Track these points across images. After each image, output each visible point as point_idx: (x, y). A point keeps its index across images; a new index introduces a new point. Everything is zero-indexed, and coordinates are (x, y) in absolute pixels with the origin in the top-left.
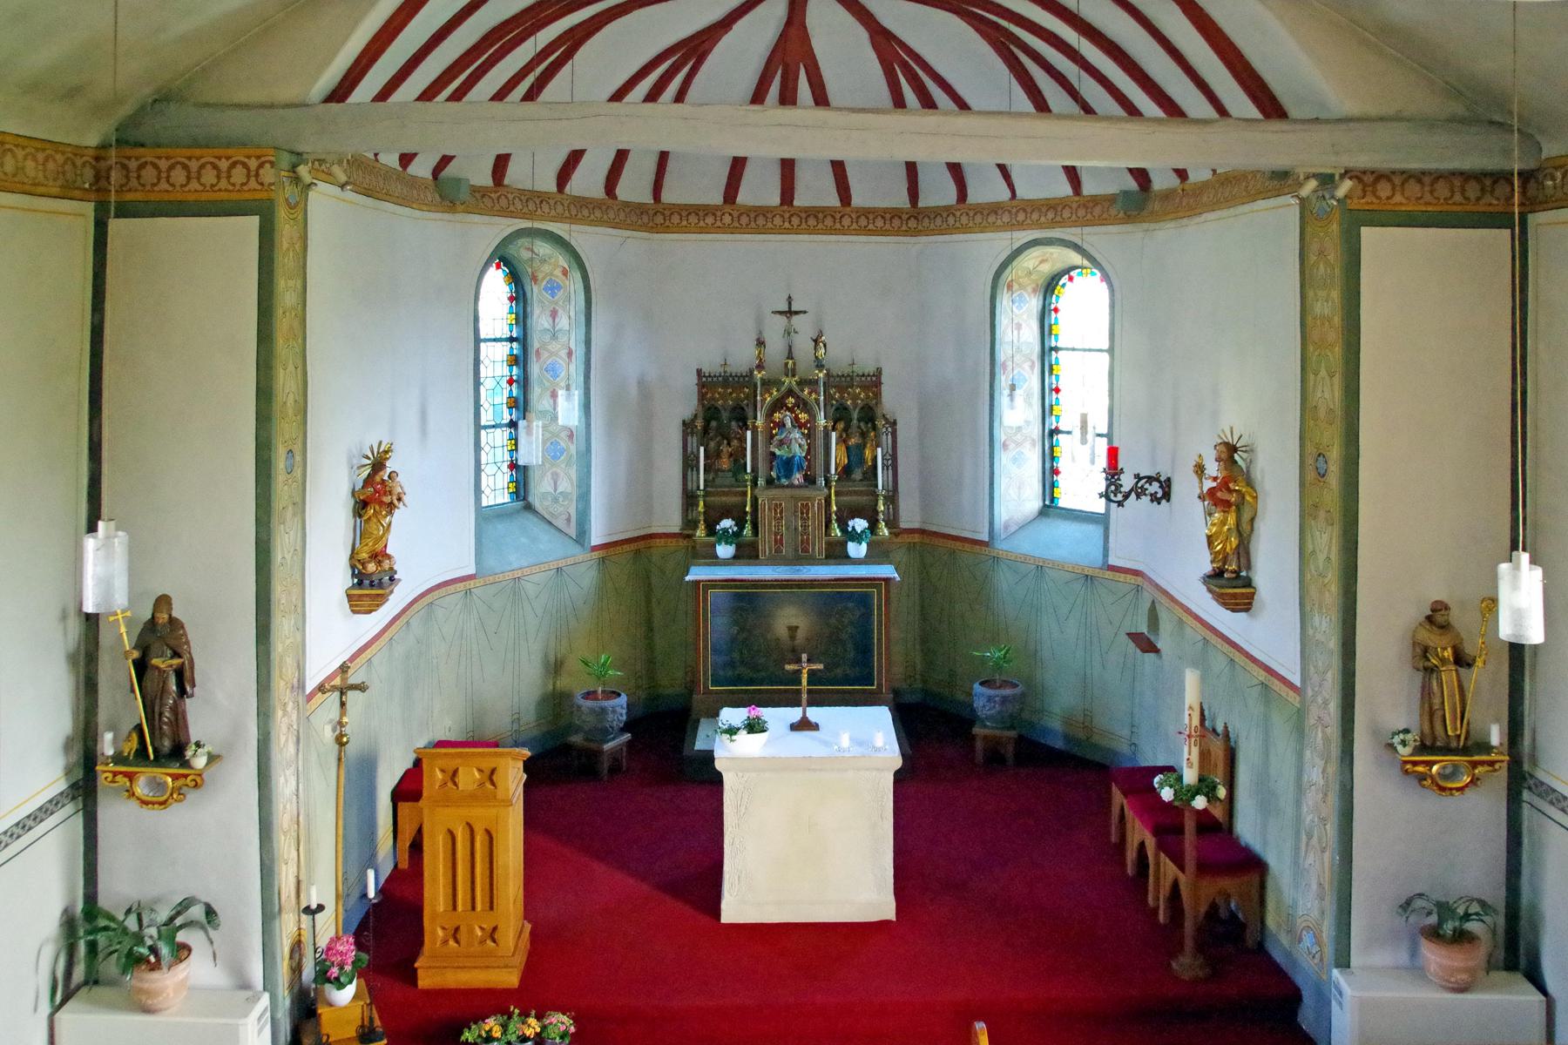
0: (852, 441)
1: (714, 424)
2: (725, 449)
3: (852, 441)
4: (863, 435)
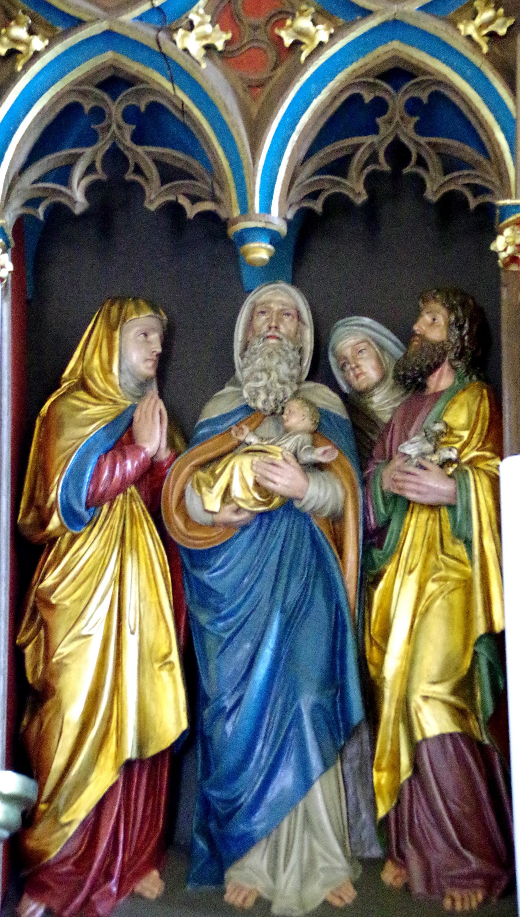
0: (227, 489)
3: (227, 489)
4: (361, 438)
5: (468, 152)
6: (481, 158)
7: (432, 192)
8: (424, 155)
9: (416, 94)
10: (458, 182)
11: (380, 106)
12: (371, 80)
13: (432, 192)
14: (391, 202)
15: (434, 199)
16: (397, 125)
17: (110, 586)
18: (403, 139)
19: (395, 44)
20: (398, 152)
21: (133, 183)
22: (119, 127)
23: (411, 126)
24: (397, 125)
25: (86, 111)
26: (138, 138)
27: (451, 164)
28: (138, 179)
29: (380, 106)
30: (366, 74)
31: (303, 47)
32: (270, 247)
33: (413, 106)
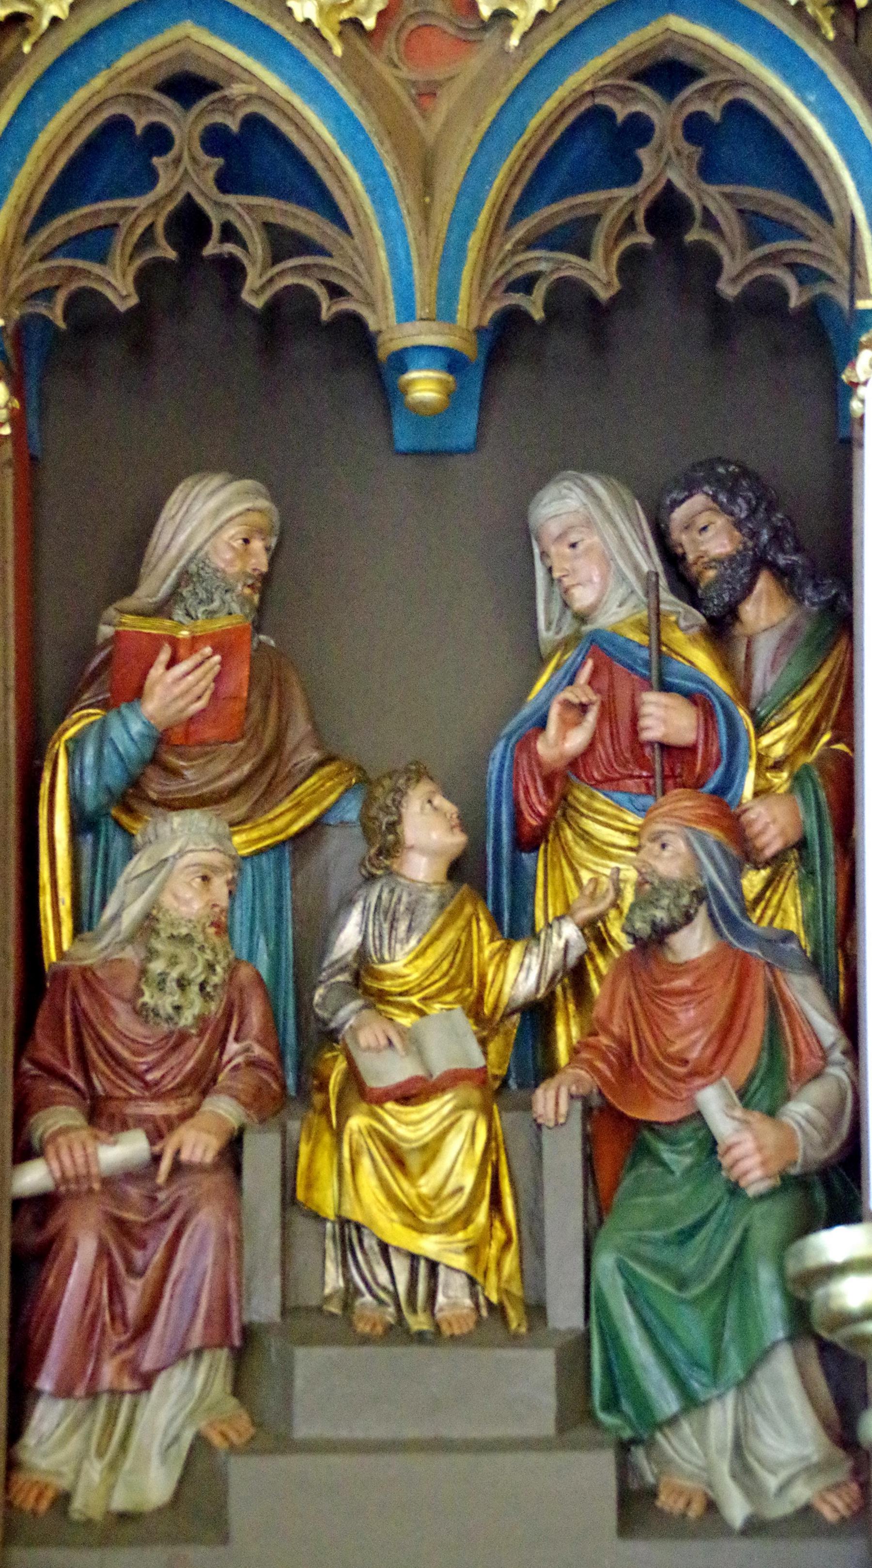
1: (211, 523)
2: (419, 971)
5: (779, 202)
6: (332, 230)
7: (254, 294)
8: (713, 208)
9: (218, 118)
10: (289, 275)
11: (639, 130)
12: (621, 82)
13: (254, 294)
14: (659, 290)
15: (258, 303)
16: (187, 173)
17: (448, 955)
18: (199, 200)
19: (678, 23)
20: (189, 223)
21: (702, 247)
22: (194, 160)
23: (211, 174)
24: (187, 173)
25: (139, 131)
26: (708, 170)
27: (284, 244)
28: (710, 237)
29: (159, 139)
30: (614, 73)
31: (513, 22)
32: (444, 376)
33: (215, 140)
